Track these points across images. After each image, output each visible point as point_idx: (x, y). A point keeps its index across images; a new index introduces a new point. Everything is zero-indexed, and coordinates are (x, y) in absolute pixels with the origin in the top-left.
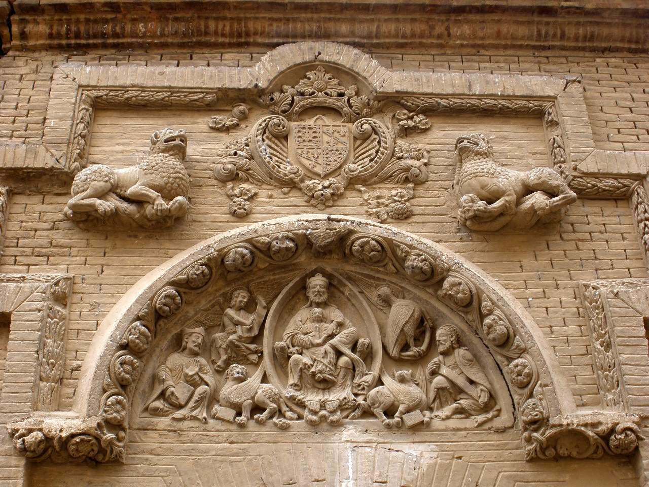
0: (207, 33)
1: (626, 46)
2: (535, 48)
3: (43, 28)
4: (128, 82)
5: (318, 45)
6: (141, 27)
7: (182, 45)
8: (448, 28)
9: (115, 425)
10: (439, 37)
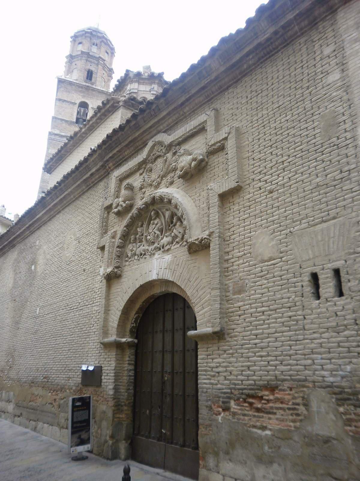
0: (138, 147)
1: (232, 82)
2: (208, 101)
3: (111, 164)
4: (123, 171)
5: (153, 139)
6: (126, 153)
7: (135, 152)
8: (183, 112)
9: (117, 267)
10: (183, 115)
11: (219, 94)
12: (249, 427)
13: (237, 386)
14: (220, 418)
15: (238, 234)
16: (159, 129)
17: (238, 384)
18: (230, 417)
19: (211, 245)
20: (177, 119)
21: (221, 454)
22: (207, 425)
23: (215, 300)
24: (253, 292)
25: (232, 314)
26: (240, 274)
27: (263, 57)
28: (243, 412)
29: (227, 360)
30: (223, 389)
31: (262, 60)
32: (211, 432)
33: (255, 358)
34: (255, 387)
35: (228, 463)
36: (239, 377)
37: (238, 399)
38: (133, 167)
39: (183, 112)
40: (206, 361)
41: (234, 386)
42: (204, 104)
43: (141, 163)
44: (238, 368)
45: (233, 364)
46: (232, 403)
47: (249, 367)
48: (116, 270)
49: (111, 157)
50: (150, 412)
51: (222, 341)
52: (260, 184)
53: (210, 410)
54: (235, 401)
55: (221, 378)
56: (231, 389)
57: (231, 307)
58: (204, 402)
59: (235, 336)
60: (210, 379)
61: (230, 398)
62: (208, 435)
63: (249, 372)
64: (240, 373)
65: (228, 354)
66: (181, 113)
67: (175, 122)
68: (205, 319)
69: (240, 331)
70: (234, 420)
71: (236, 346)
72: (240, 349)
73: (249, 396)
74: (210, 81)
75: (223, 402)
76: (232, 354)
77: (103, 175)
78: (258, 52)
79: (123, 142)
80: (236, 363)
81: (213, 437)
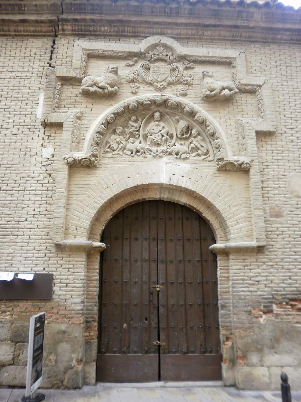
0: (124, 32)
7: (116, 36)
8: (203, 33)
10: (200, 35)
11: (245, 41)
12: (293, 324)
13: (279, 293)
14: (262, 320)
15: (273, 170)
16: (165, 31)
17: (281, 291)
18: (273, 318)
19: (251, 170)
21: (266, 350)
22: (246, 328)
23: (259, 218)
24: (291, 218)
25: (270, 233)
26: (277, 202)
27: (294, 40)
28: (286, 313)
29: (267, 270)
30: (264, 295)
31: (292, 42)
32: (252, 333)
33: (296, 270)
34: (298, 293)
35: (273, 355)
36: (281, 285)
37: (281, 303)
38: (119, 52)
39: (203, 33)
40: (243, 271)
41: (276, 293)
42: (227, 40)
43: (132, 54)
44: (279, 278)
45: (273, 274)
46: (275, 307)
47: (290, 277)
49: (76, 20)
50: (129, 325)
51: (261, 254)
52: (292, 138)
53: (250, 314)
54: (276, 304)
55: (262, 286)
56: (272, 295)
57: (269, 227)
58: (242, 308)
59: (275, 251)
60: (247, 287)
61: (272, 302)
62: (249, 336)
63: (290, 281)
64: (282, 281)
65: (267, 266)
66: (200, 33)
67: (188, 36)
68: (242, 234)
69: (280, 248)
70: (277, 320)
71: (276, 259)
72: (280, 262)
73: (291, 300)
74: (247, 26)
75: (265, 307)
76: (272, 266)
77: (44, 32)
78: (294, 33)
79: (106, 14)
80: (277, 273)
81: (255, 337)
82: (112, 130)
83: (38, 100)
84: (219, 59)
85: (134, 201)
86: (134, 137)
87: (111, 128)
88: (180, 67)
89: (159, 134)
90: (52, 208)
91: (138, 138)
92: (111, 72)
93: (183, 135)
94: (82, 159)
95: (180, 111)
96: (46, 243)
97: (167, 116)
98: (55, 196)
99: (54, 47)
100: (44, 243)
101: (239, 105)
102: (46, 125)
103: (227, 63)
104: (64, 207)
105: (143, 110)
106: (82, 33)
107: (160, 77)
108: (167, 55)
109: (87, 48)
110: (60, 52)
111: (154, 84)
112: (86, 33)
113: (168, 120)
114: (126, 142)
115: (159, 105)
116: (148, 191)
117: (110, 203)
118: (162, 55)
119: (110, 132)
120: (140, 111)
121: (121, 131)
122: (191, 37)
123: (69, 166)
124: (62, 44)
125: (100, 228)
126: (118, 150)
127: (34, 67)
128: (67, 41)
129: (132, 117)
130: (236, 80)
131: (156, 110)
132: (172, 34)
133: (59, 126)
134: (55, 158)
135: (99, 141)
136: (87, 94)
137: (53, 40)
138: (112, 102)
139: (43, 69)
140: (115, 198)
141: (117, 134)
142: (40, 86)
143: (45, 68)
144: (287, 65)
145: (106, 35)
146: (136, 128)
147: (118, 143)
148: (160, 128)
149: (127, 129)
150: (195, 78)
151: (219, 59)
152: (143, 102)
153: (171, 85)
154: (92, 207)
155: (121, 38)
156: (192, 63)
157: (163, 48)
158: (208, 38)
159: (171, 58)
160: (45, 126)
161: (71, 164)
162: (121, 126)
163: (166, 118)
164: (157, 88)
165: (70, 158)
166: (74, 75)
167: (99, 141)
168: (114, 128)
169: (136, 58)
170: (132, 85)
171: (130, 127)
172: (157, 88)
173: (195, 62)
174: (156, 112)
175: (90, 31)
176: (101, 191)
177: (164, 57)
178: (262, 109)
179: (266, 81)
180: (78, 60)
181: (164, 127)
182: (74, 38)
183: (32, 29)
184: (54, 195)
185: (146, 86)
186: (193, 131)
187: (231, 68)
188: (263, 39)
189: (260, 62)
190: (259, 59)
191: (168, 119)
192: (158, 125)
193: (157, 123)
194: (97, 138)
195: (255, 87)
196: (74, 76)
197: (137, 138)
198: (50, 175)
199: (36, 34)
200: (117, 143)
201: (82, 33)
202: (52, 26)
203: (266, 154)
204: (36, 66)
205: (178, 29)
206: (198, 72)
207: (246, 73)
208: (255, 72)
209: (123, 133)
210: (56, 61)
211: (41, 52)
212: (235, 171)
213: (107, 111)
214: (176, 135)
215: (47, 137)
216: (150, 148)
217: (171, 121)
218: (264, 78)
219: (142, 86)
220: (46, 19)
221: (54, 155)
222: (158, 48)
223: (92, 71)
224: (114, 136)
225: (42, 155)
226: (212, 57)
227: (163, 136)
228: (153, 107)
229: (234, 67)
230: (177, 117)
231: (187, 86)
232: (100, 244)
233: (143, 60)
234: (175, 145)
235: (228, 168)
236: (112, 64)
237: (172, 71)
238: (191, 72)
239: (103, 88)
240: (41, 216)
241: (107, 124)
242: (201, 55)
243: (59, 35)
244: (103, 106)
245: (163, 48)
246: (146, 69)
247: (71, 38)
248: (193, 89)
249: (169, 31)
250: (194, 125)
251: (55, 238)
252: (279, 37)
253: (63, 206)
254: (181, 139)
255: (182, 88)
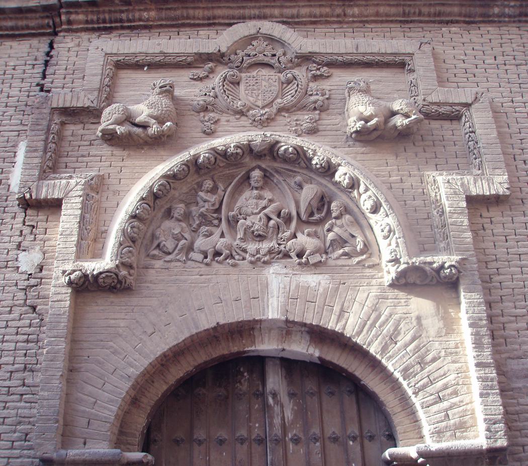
0: (134, 21)
10: (338, 16)
20: (321, 16)
25: (515, 417)
38: (178, 55)
39: (344, 11)
48: (124, 272)
66: (339, 11)
77: (33, 28)
82: (163, 210)
83: (15, 156)
84: (379, 58)
85: (213, 360)
86: (210, 223)
87: (162, 207)
88: (301, 76)
89: (261, 214)
90: (39, 377)
91: (218, 226)
92: (159, 94)
93: (312, 214)
94: (101, 273)
95: (303, 164)
96: (20, 457)
97: (277, 176)
98: (42, 354)
99: (52, 54)
100: (17, 458)
101: (428, 146)
102: (27, 204)
103: (399, 64)
104: (61, 375)
105: (229, 166)
106: (105, 25)
107: (260, 98)
108: (274, 55)
109: (115, 51)
110: (63, 63)
111: (248, 114)
112: (113, 25)
113: (280, 186)
114: (193, 234)
115: (259, 156)
116: (241, 336)
117: (162, 365)
118: (264, 55)
119: (160, 215)
120: (221, 170)
121: (182, 212)
122: (320, 21)
123: (73, 289)
124: (66, 45)
125: (140, 421)
126: (176, 251)
127: (11, 94)
128: (77, 42)
129: (205, 182)
130: (417, 96)
131: (254, 165)
132: (282, 16)
133: (55, 205)
134: (44, 272)
135: (135, 235)
136: (110, 138)
137: (49, 41)
138: (162, 153)
139: (28, 96)
140: (171, 354)
141: (174, 219)
142: (21, 128)
143: (32, 94)
144: (518, 62)
145: (151, 25)
146: (213, 205)
147: (177, 238)
148: (264, 203)
149: (194, 208)
150: (333, 96)
151: (379, 58)
152: (226, 151)
153: (283, 114)
154: (121, 376)
155: (182, 30)
156: (325, 68)
157: (265, 43)
158: (355, 19)
159: (282, 59)
160: (26, 207)
161: (77, 284)
162: (182, 201)
163: (275, 181)
164: (254, 120)
165: (74, 271)
166: (87, 104)
167: (135, 235)
168: (168, 206)
169: (211, 65)
170: (204, 117)
171: (201, 203)
172: (254, 120)
173: (332, 65)
174: (253, 169)
175: (121, 21)
176: (141, 339)
177: (266, 60)
178: (475, 152)
179: (479, 96)
180: (94, 75)
181: (271, 201)
182: (89, 36)
183: (10, 24)
184: (40, 351)
185: (232, 118)
186: (333, 204)
187: (406, 72)
188: (465, 16)
189: (464, 61)
190: (461, 54)
191: (280, 183)
192: (260, 197)
193: (255, 192)
194: (131, 228)
195: (457, 108)
196: (86, 106)
197: (215, 226)
198: (34, 308)
199: (17, 33)
200: (174, 238)
201: (105, 25)
202: (47, 17)
203: (504, 238)
204: (15, 92)
205: (294, 7)
206: (339, 83)
207: (436, 82)
208: (456, 79)
209: (187, 216)
210: (55, 80)
211: (26, 65)
212: (426, 284)
213: (155, 170)
214: (298, 215)
215: (29, 229)
216: (244, 245)
217: (286, 187)
218: (475, 90)
219: (224, 118)
220: (38, 4)
221: (42, 266)
222: (254, 43)
223: (124, 94)
224: (167, 224)
225: (18, 268)
226: (364, 54)
227: (269, 219)
228: (247, 160)
229: (412, 71)
230: (298, 178)
231: (317, 112)
232: (137, 455)
233: (226, 67)
234: (295, 236)
235: (411, 280)
236: (160, 78)
237: (285, 85)
238: (325, 85)
239: (144, 126)
240: (12, 397)
241: (151, 199)
242: (343, 51)
243: (61, 31)
244: (143, 163)
245: (265, 43)
246: (232, 83)
247: (85, 36)
248: (330, 117)
249: (276, 12)
250: (334, 192)
251: (41, 445)
252: (496, 10)
253: (60, 373)
254: (308, 223)
255: (307, 117)
